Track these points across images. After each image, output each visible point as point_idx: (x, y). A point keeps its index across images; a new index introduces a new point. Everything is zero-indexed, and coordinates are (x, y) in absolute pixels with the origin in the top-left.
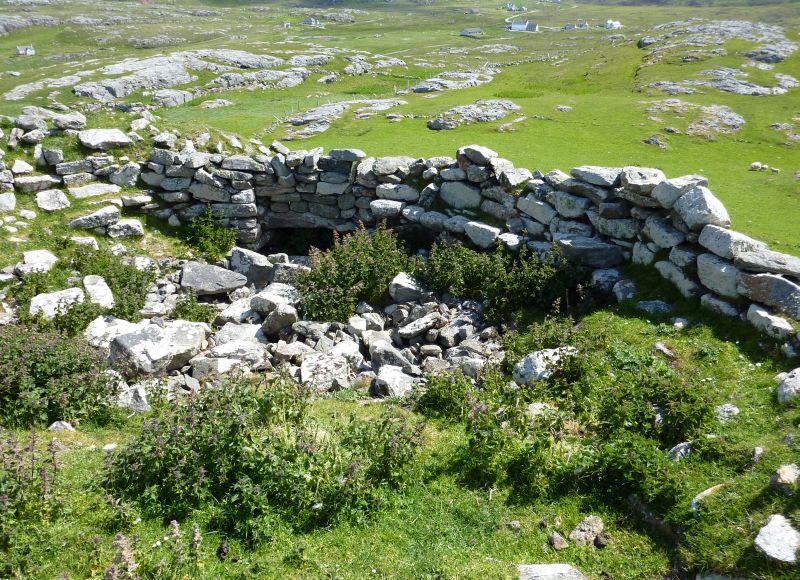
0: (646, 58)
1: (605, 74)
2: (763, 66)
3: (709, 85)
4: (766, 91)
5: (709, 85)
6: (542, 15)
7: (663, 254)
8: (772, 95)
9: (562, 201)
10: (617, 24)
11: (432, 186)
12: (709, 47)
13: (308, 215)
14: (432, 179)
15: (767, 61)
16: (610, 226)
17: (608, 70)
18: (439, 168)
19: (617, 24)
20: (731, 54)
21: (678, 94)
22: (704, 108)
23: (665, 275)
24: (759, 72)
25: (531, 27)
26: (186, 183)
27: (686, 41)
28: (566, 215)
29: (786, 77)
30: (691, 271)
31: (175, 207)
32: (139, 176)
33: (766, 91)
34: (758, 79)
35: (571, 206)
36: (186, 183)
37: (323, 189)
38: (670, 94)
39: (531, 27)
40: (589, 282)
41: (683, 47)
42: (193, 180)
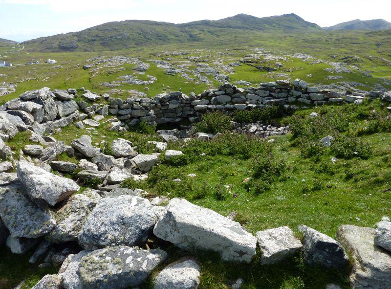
0: (91, 74)
1: (74, 83)
2: (141, 73)
3: (124, 82)
4: (146, 82)
5: (124, 82)
6: (11, 58)
7: (299, 97)
8: (150, 84)
9: (262, 93)
10: (54, 61)
11: (213, 98)
12: (117, 67)
13: (164, 118)
14: (212, 96)
15: (142, 71)
16: (280, 95)
17: (75, 80)
18: (214, 92)
19: (54, 61)
20: (127, 69)
21: (114, 87)
22: (128, 91)
23: (302, 101)
24: (141, 75)
25: (8, 65)
26: (130, 110)
27: (106, 65)
28: (264, 95)
29: (151, 76)
30: (309, 98)
31: (126, 121)
32: (109, 111)
33: (146, 82)
34: (141, 78)
35: (265, 93)
36: (130, 110)
37: (172, 106)
38: (111, 87)
39: (8, 65)
40: (24, 286)
41: (106, 68)
42: (133, 109)
